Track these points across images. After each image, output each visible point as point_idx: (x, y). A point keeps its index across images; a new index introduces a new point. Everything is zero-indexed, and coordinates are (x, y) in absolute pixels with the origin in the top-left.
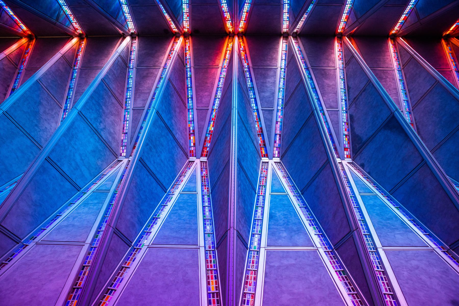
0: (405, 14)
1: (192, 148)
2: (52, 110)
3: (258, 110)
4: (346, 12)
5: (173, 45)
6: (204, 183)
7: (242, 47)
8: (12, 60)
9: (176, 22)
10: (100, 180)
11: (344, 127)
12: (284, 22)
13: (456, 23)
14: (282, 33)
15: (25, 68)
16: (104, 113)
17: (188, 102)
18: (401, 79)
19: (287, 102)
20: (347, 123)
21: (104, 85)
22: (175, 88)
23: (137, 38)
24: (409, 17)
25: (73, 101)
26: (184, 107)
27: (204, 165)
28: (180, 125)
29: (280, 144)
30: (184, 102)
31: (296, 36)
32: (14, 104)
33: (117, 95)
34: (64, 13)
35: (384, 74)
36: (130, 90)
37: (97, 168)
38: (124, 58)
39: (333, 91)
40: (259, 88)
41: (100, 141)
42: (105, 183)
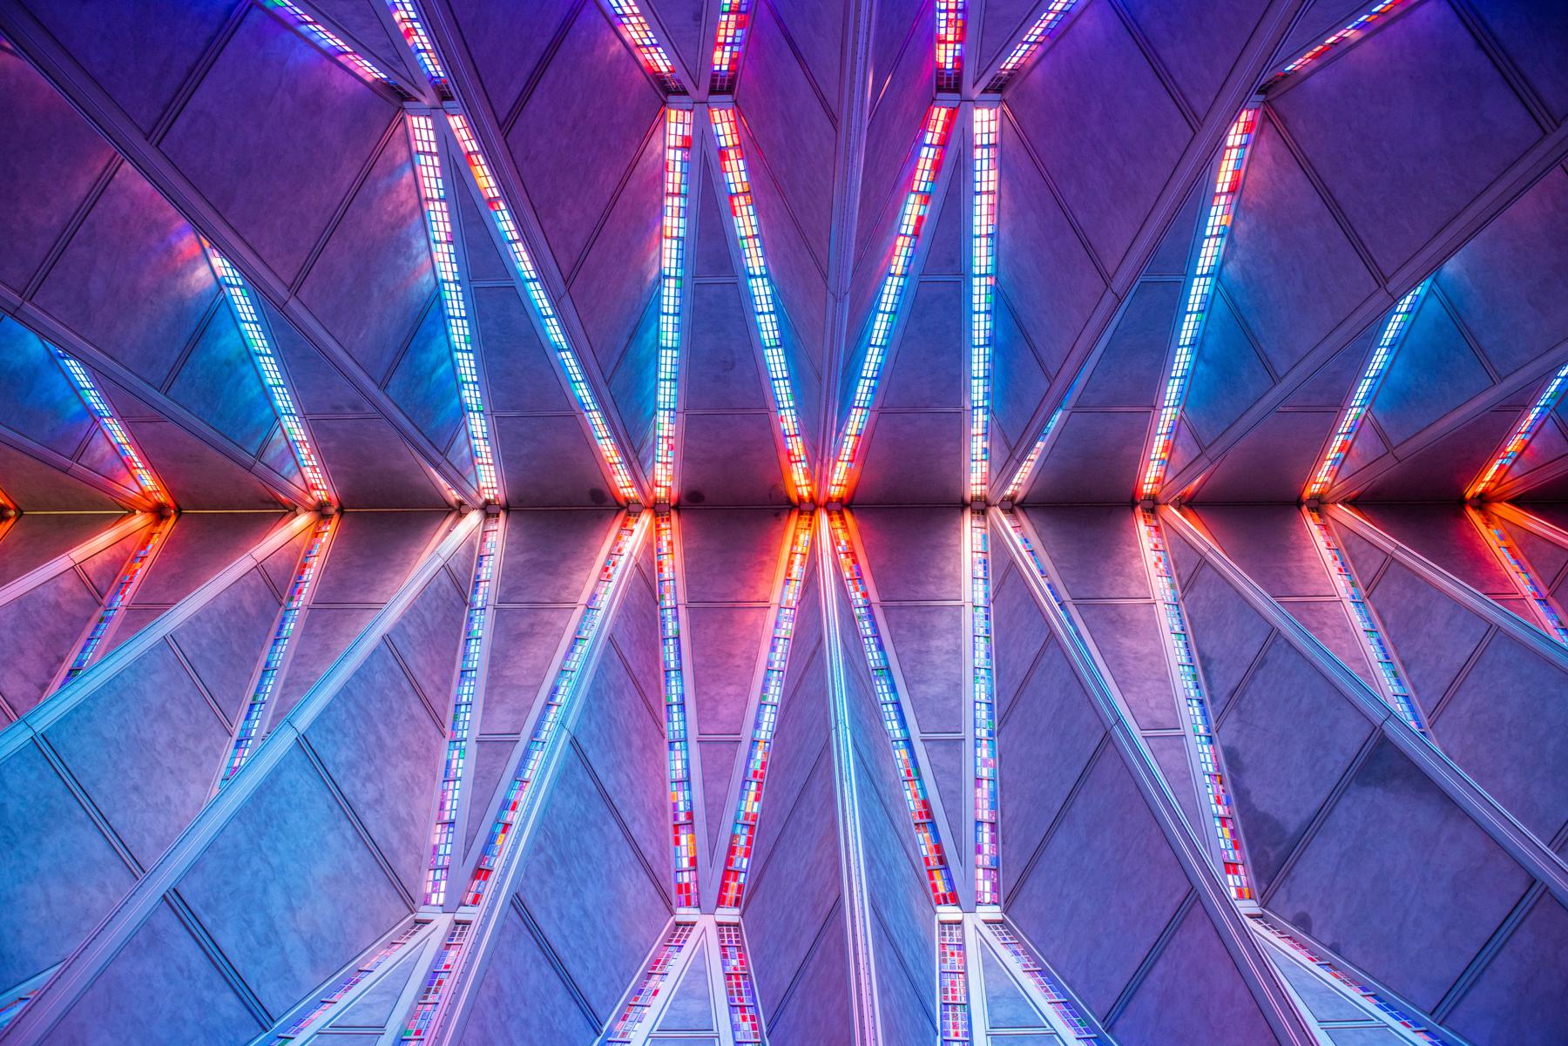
0: (1342, 433)
1: (686, 874)
2: (198, 738)
3: (908, 742)
4: (1164, 431)
5: (618, 537)
6: (739, 999)
7: (843, 543)
8: (91, 576)
9: (635, 465)
10: (346, 991)
11: (1210, 790)
12: (974, 464)
13: (1499, 458)
14: (968, 498)
15: (126, 602)
16: (381, 746)
17: (669, 720)
18: (1368, 627)
19: (1006, 712)
20: (1218, 777)
21: (390, 654)
22: (628, 669)
23: (502, 515)
24: (1356, 443)
25: (276, 709)
26: (656, 733)
27: (729, 936)
28: (645, 792)
29: (997, 857)
30: (654, 714)
31: (1013, 507)
32: (77, 710)
33: (429, 690)
34: (282, 437)
35: (1311, 615)
36: (471, 679)
37: (339, 943)
38: (458, 576)
39: (1155, 673)
40: (907, 668)
41: (360, 845)
42: (367, 1001)
